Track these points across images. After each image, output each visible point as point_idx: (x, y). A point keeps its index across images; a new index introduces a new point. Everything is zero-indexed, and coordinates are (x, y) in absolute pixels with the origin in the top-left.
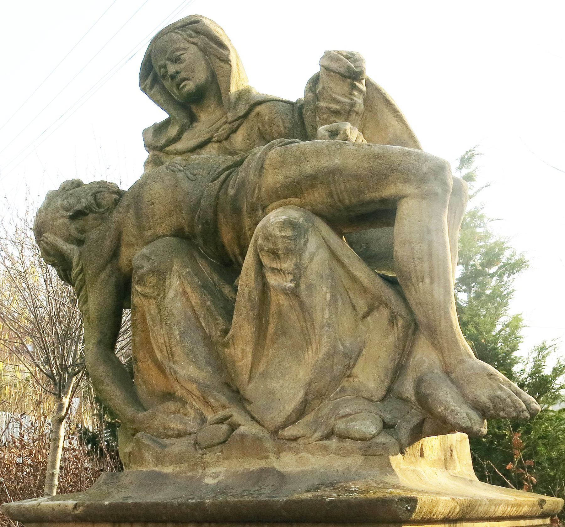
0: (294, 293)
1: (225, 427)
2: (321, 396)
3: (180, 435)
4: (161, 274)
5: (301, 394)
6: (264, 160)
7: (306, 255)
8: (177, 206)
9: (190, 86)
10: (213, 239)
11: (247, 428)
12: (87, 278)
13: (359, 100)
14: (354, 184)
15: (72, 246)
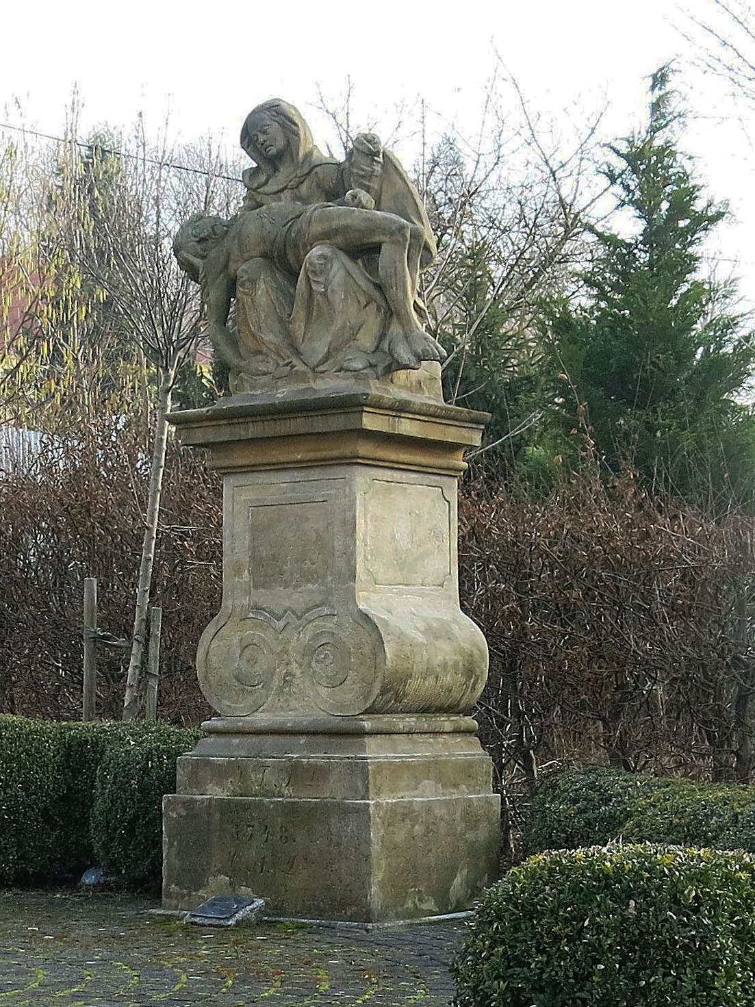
0: (324, 295)
1: (289, 368)
2: (337, 350)
3: (265, 374)
4: (254, 282)
5: (326, 348)
6: (311, 217)
7: (332, 273)
8: (263, 239)
9: (273, 151)
10: (283, 260)
11: (300, 367)
12: (209, 280)
13: (378, 168)
14: (357, 235)
15: (198, 260)
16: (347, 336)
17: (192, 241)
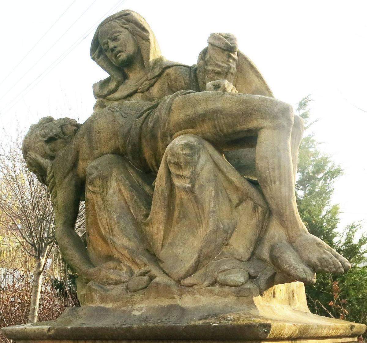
0: (191, 191)
1: (146, 278)
2: (208, 257)
3: (117, 283)
4: (105, 179)
6: (171, 104)
7: (199, 166)
8: (115, 134)
9: (123, 56)
10: (139, 156)
11: (160, 278)
12: (57, 181)
13: (233, 65)
14: (230, 120)
15: (47, 160)
16: (220, 240)
17: (41, 141)
